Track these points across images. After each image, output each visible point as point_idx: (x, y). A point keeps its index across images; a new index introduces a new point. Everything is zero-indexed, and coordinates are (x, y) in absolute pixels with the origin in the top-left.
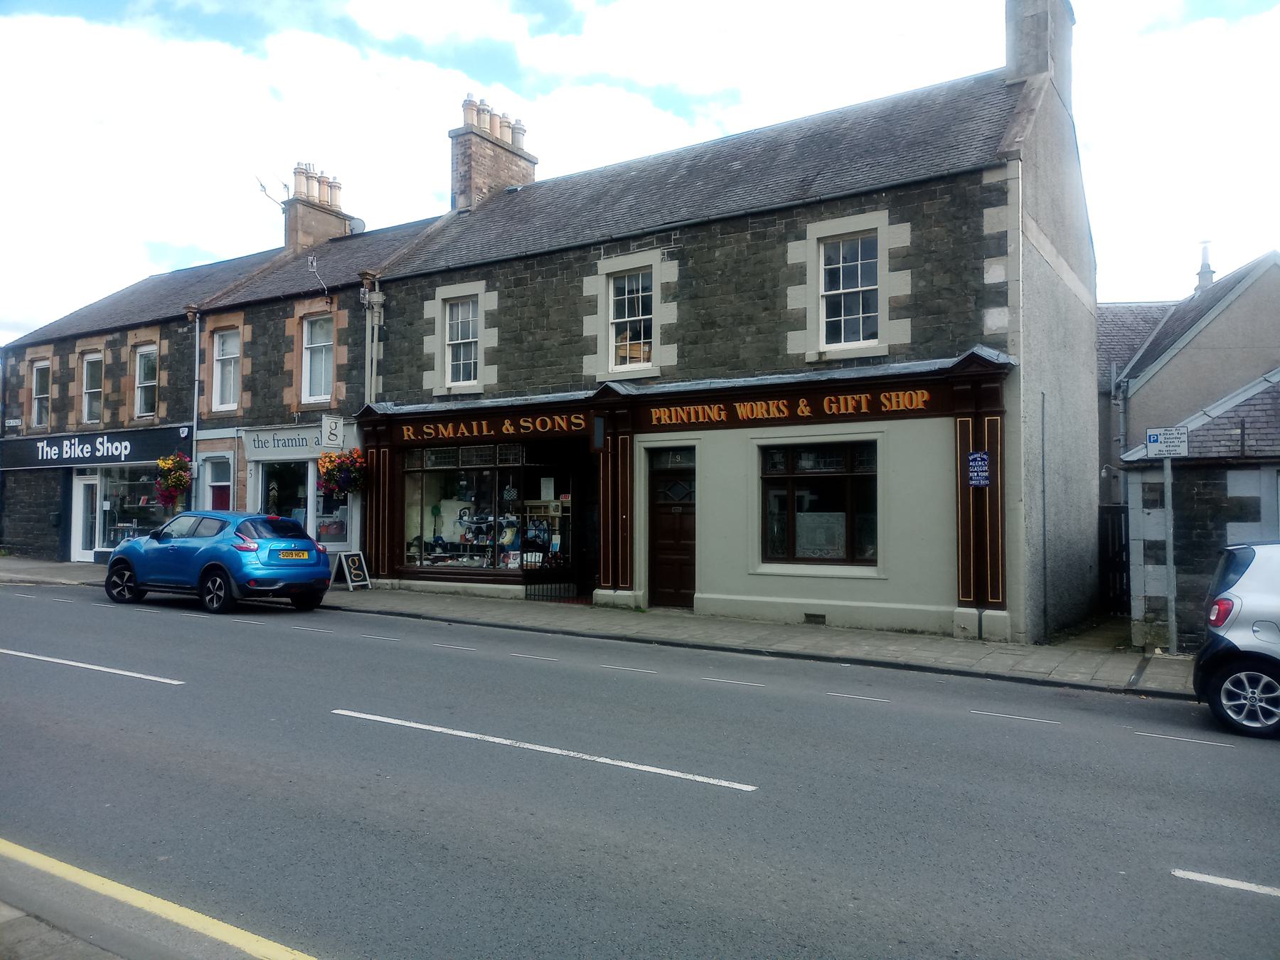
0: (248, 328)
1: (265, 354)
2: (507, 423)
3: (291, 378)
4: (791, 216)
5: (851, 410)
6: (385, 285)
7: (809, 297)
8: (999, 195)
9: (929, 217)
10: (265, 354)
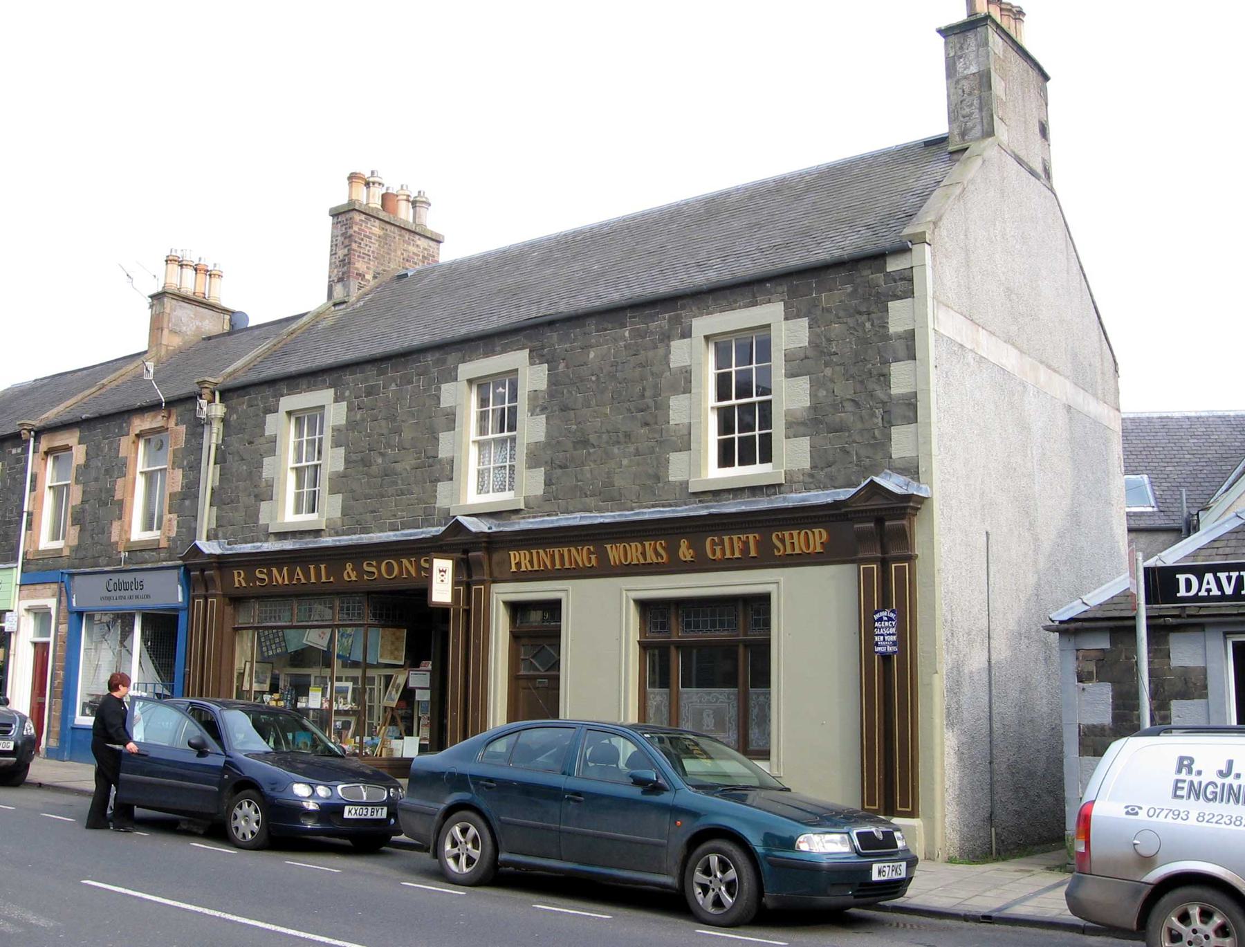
0: (83, 448)
1: (96, 480)
2: (349, 567)
3: (121, 509)
4: (677, 304)
5: (737, 555)
6: (227, 394)
7: (701, 413)
8: (905, 286)
9: (828, 310)
10: (96, 480)
